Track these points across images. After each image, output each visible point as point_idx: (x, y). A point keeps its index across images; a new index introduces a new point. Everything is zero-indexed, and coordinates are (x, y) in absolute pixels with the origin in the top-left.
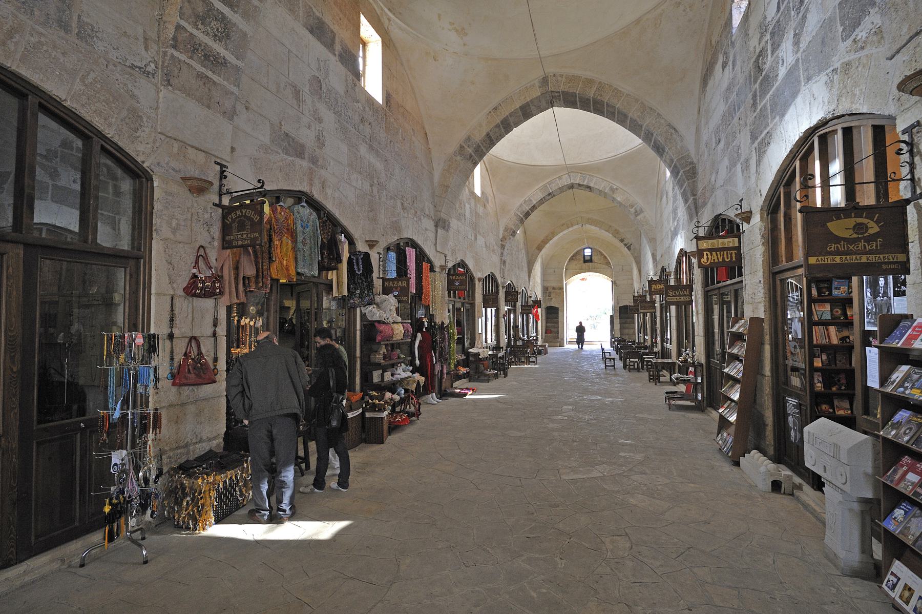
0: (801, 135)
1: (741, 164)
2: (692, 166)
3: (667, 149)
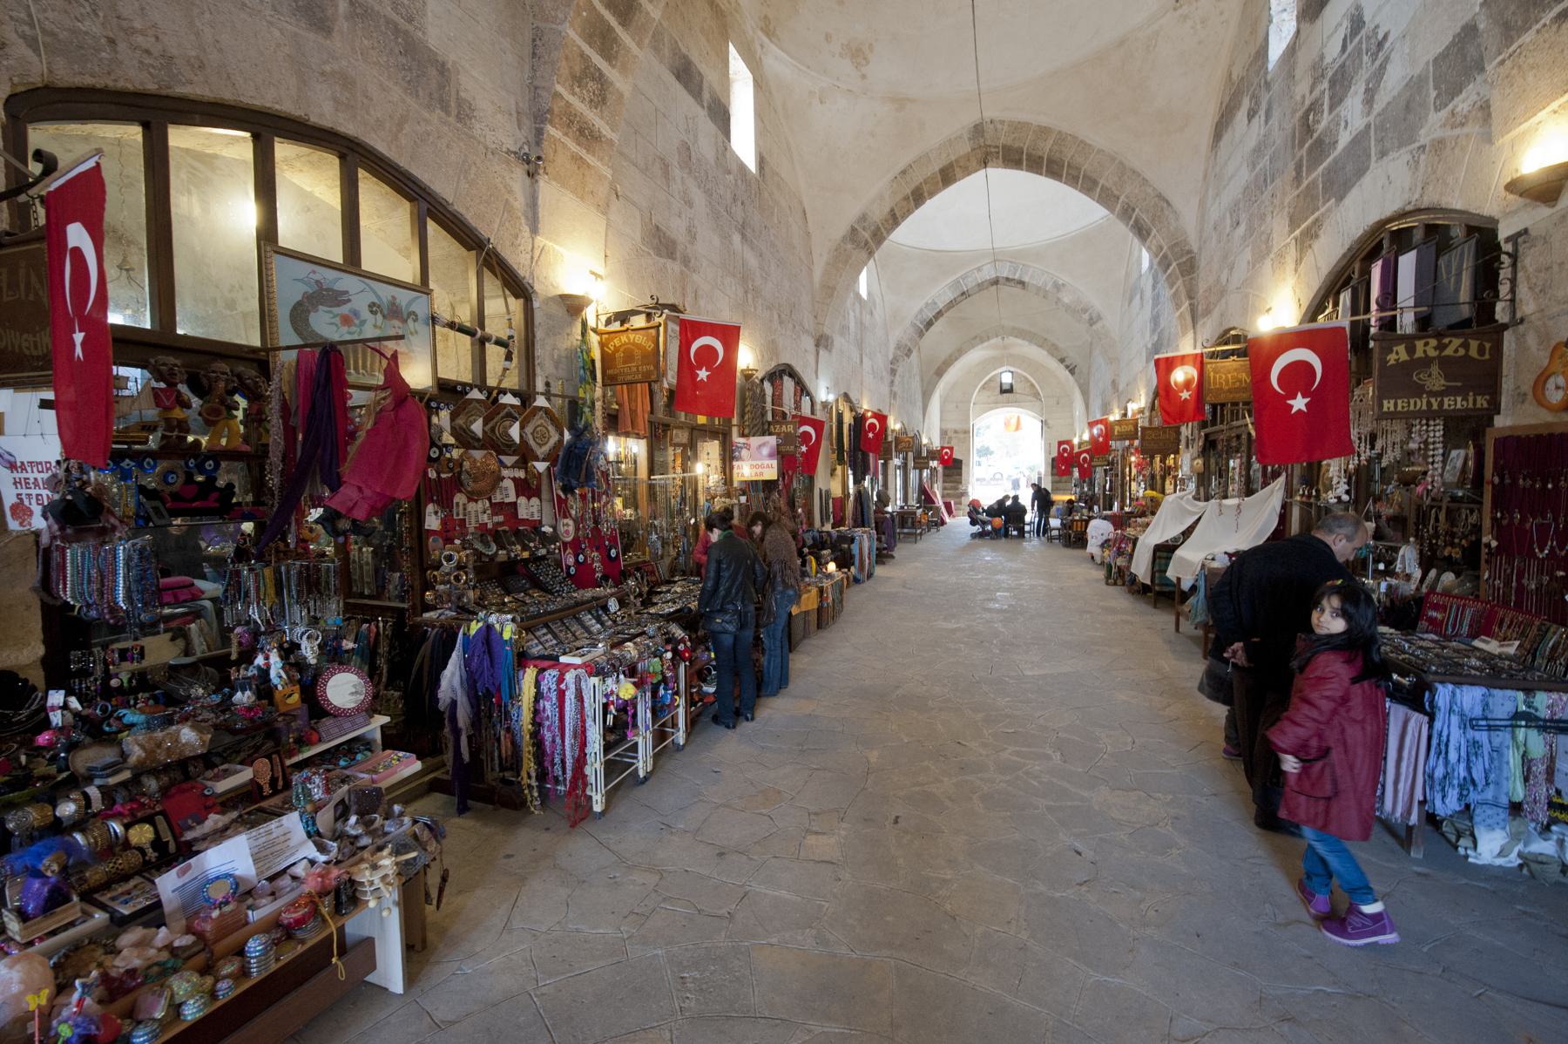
3: (1154, 231)
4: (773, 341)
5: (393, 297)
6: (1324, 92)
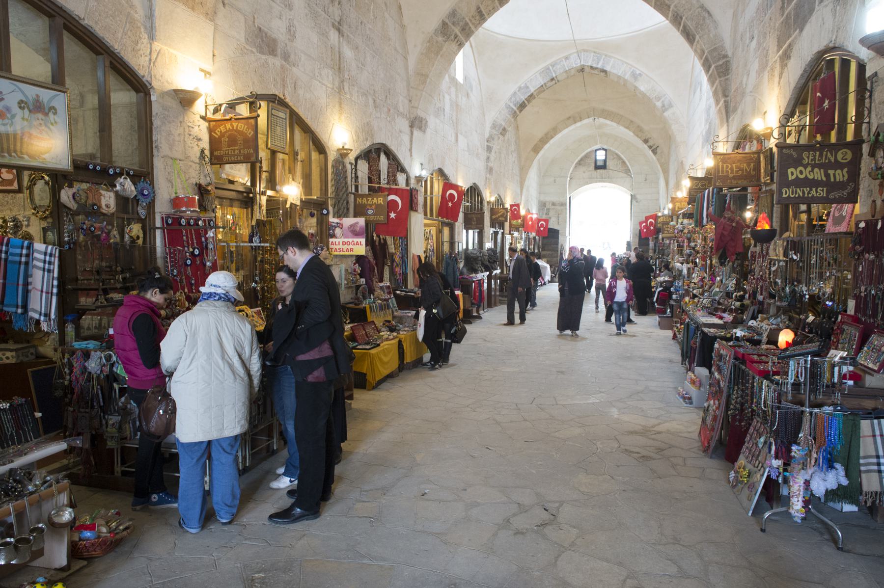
0: (812, 57)
1: (768, 72)
3: (697, 37)
5: (38, 96)
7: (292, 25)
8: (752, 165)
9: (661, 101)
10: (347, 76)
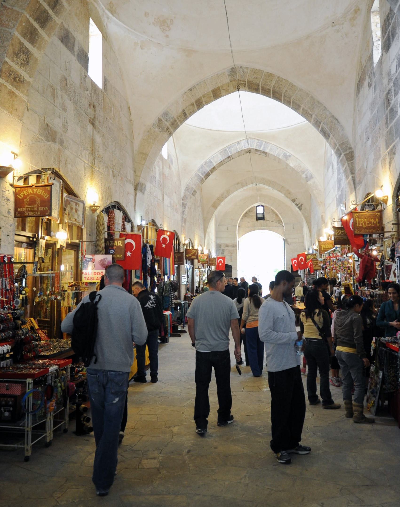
1: (381, 161)
2: (350, 150)
4: (109, 188)
6: (392, 87)
7: (66, 121)
8: (377, 219)
9: (305, 174)
10: (97, 156)
